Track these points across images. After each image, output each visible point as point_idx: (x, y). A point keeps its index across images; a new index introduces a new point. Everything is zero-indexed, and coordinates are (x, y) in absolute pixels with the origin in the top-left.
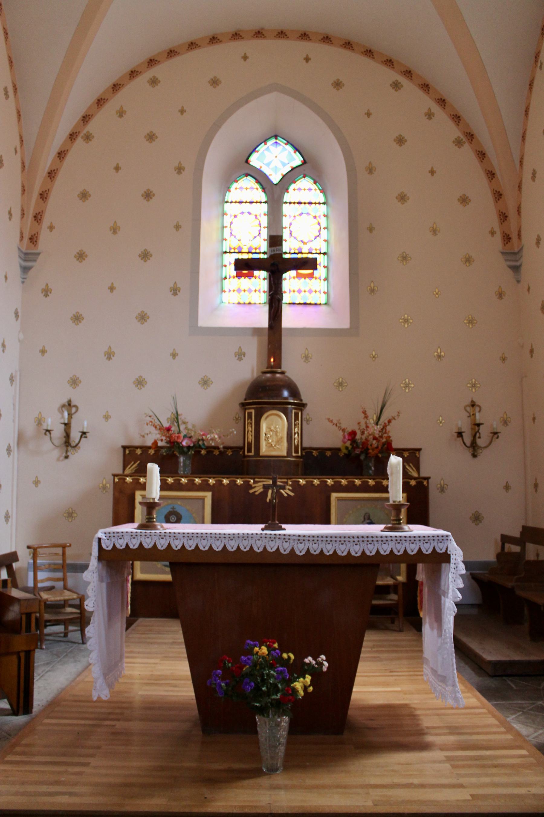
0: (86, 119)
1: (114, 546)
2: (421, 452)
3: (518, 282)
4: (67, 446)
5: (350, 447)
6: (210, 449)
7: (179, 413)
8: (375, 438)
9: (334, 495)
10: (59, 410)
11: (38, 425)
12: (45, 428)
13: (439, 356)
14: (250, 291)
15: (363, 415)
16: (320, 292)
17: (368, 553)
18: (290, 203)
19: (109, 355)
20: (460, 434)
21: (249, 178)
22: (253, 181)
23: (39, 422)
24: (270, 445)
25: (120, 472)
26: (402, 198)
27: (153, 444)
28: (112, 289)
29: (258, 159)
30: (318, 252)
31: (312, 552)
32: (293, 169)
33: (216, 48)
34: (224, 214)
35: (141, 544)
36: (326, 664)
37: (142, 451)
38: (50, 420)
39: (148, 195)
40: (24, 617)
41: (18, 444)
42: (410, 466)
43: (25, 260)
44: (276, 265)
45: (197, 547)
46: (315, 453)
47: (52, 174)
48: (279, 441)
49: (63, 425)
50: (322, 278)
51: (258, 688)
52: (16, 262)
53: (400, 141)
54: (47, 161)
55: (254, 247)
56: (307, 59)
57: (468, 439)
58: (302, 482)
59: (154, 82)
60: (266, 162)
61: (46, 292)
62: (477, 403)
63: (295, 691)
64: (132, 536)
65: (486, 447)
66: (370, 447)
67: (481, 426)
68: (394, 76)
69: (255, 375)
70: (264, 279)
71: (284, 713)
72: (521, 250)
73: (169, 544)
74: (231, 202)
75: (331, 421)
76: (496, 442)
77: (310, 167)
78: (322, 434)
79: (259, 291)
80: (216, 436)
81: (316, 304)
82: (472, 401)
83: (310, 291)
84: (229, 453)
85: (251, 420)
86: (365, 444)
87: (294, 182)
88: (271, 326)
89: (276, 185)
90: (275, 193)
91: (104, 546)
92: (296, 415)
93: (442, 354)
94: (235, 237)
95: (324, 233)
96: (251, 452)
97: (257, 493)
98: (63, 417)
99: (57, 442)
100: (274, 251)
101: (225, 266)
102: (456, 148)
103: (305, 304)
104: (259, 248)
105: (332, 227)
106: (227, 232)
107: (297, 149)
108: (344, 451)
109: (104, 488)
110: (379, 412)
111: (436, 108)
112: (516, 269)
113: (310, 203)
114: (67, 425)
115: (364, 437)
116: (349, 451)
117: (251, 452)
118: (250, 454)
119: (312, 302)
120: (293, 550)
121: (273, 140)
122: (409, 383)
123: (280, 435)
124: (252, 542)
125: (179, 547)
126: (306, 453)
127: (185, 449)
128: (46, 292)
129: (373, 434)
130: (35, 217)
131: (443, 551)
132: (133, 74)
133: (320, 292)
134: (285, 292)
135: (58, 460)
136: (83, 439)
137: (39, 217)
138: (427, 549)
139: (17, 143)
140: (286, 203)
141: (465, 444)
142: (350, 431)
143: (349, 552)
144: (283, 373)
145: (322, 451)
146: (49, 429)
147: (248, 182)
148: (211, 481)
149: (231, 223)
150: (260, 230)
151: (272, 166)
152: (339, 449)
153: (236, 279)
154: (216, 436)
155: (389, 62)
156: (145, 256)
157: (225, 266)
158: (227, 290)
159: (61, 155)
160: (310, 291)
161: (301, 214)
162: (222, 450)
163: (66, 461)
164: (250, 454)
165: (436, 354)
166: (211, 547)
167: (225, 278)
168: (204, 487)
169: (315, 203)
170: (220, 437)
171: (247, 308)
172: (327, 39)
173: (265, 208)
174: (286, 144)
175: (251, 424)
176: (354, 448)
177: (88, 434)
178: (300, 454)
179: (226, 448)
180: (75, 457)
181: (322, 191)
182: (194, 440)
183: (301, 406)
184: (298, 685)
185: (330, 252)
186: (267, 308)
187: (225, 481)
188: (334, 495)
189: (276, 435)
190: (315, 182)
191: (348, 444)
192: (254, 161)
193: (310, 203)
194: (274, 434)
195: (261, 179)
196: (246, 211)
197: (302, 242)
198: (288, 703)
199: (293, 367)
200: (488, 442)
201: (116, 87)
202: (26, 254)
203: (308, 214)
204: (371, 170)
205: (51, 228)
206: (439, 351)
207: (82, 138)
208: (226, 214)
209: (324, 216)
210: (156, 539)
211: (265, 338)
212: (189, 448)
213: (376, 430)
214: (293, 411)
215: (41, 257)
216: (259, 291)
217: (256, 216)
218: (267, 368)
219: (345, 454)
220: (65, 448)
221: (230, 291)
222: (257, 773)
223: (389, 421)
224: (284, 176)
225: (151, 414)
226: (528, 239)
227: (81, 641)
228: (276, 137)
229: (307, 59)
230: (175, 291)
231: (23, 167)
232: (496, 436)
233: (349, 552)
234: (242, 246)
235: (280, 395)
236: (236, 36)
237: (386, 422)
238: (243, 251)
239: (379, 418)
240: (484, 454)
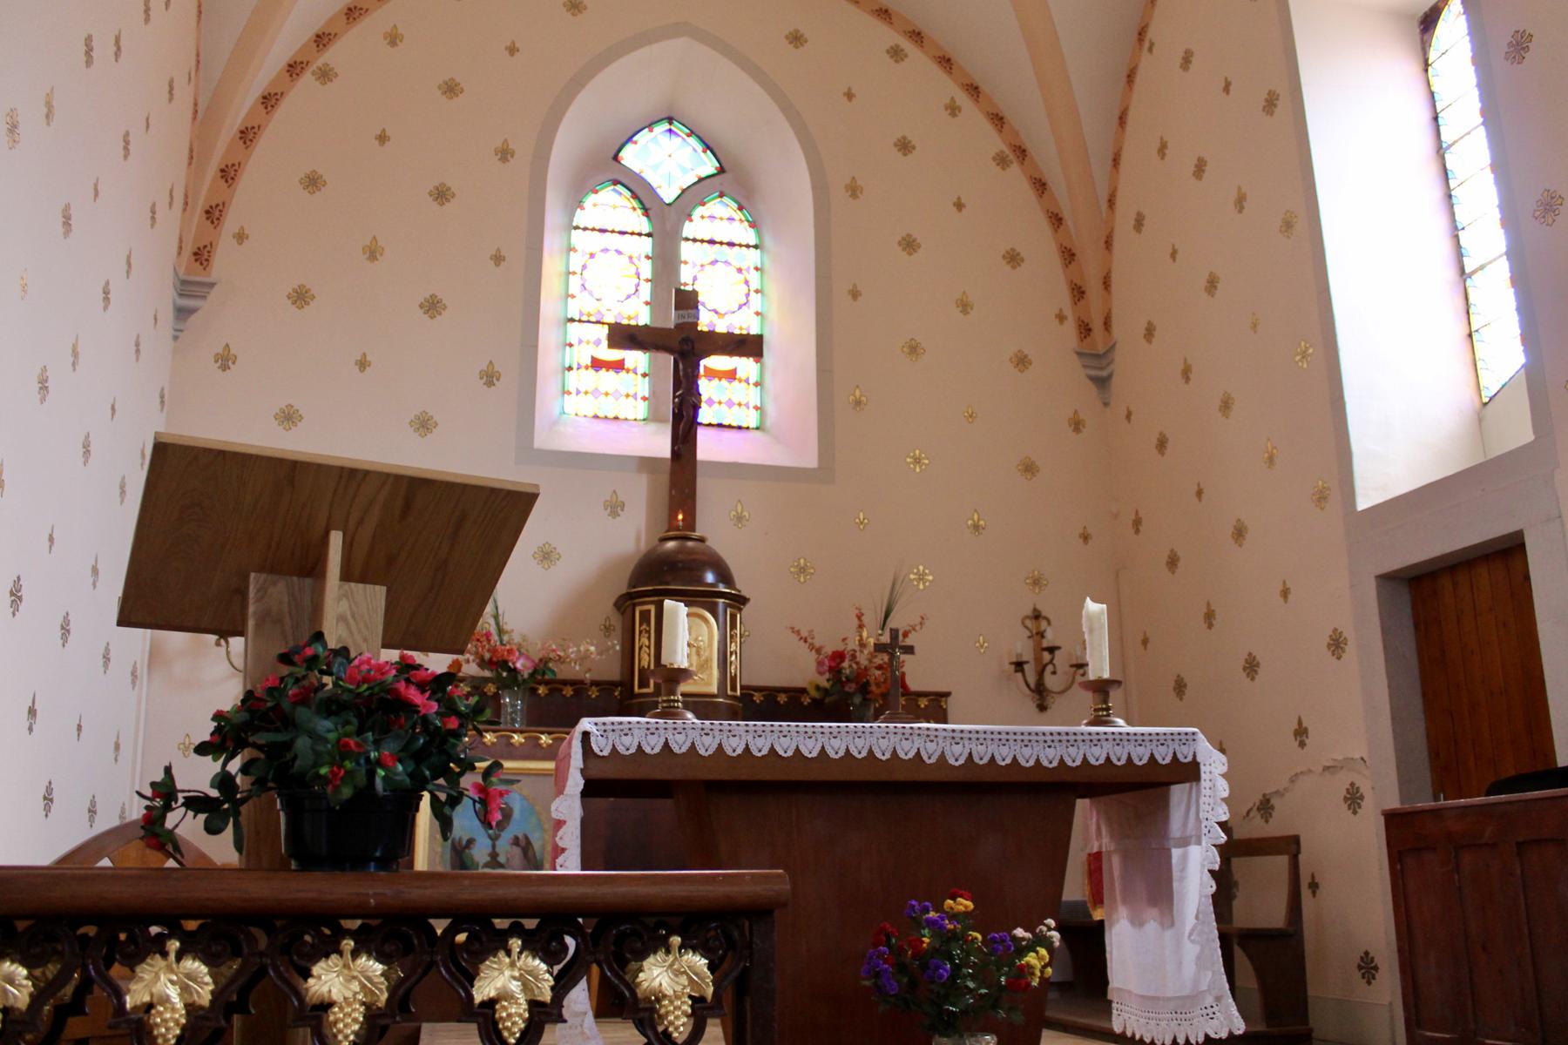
0: (322, 40)
2: (950, 699)
3: (1106, 404)
13: (976, 527)
20: (1019, 666)
28: (363, 364)
32: (701, 180)
34: (571, 249)
35: (666, 744)
43: (181, 295)
44: (680, 344)
45: (772, 750)
47: (247, 135)
50: (752, 381)
52: (167, 299)
61: (225, 360)
65: (1063, 692)
67: (1057, 653)
68: (892, 37)
69: (643, 547)
70: (644, 375)
73: (720, 745)
77: (730, 178)
81: (740, 428)
82: (1035, 610)
83: (730, 404)
85: (649, 625)
92: (733, 617)
94: (591, 293)
95: (754, 298)
96: (647, 686)
101: (571, 345)
102: (998, 169)
103: (720, 425)
105: (772, 289)
106: (575, 282)
107: (708, 147)
111: (963, 99)
112: (1102, 383)
113: (731, 244)
117: (647, 686)
118: (645, 690)
119: (734, 424)
120: (943, 756)
121: (666, 126)
123: (705, 655)
125: (739, 751)
128: (225, 360)
130: (207, 212)
131: (1190, 759)
139: (193, 63)
140: (687, 239)
144: (702, 540)
149: (584, 267)
152: (803, 691)
153: (591, 371)
156: (432, 306)
157: (571, 345)
158: (574, 392)
159: (269, 101)
160: (730, 404)
161: (714, 263)
164: (645, 690)
166: (797, 750)
167: (570, 369)
171: (613, 426)
173: (646, 245)
175: (648, 632)
181: (752, 225)
189: (698, 654)
190: (741, 208)
192: (629, 157)
193: (731, 244)
195: (642, 194)
196: (612, 247)
199: (717, 525)
200: (1062, 688)
202: (184, 282)
204: (854, 190)
205: (241, 237)
207: (313, 73)
208: (575, 250)
209: (757, 269)
211: (665, 479)
215: (214, 294)
219: (814, 700)
221: (578, 392)
224: (684, 191)
226: (1126, 329)
228: (670, 120)
230: (490, 378)
233: (1038, 760)
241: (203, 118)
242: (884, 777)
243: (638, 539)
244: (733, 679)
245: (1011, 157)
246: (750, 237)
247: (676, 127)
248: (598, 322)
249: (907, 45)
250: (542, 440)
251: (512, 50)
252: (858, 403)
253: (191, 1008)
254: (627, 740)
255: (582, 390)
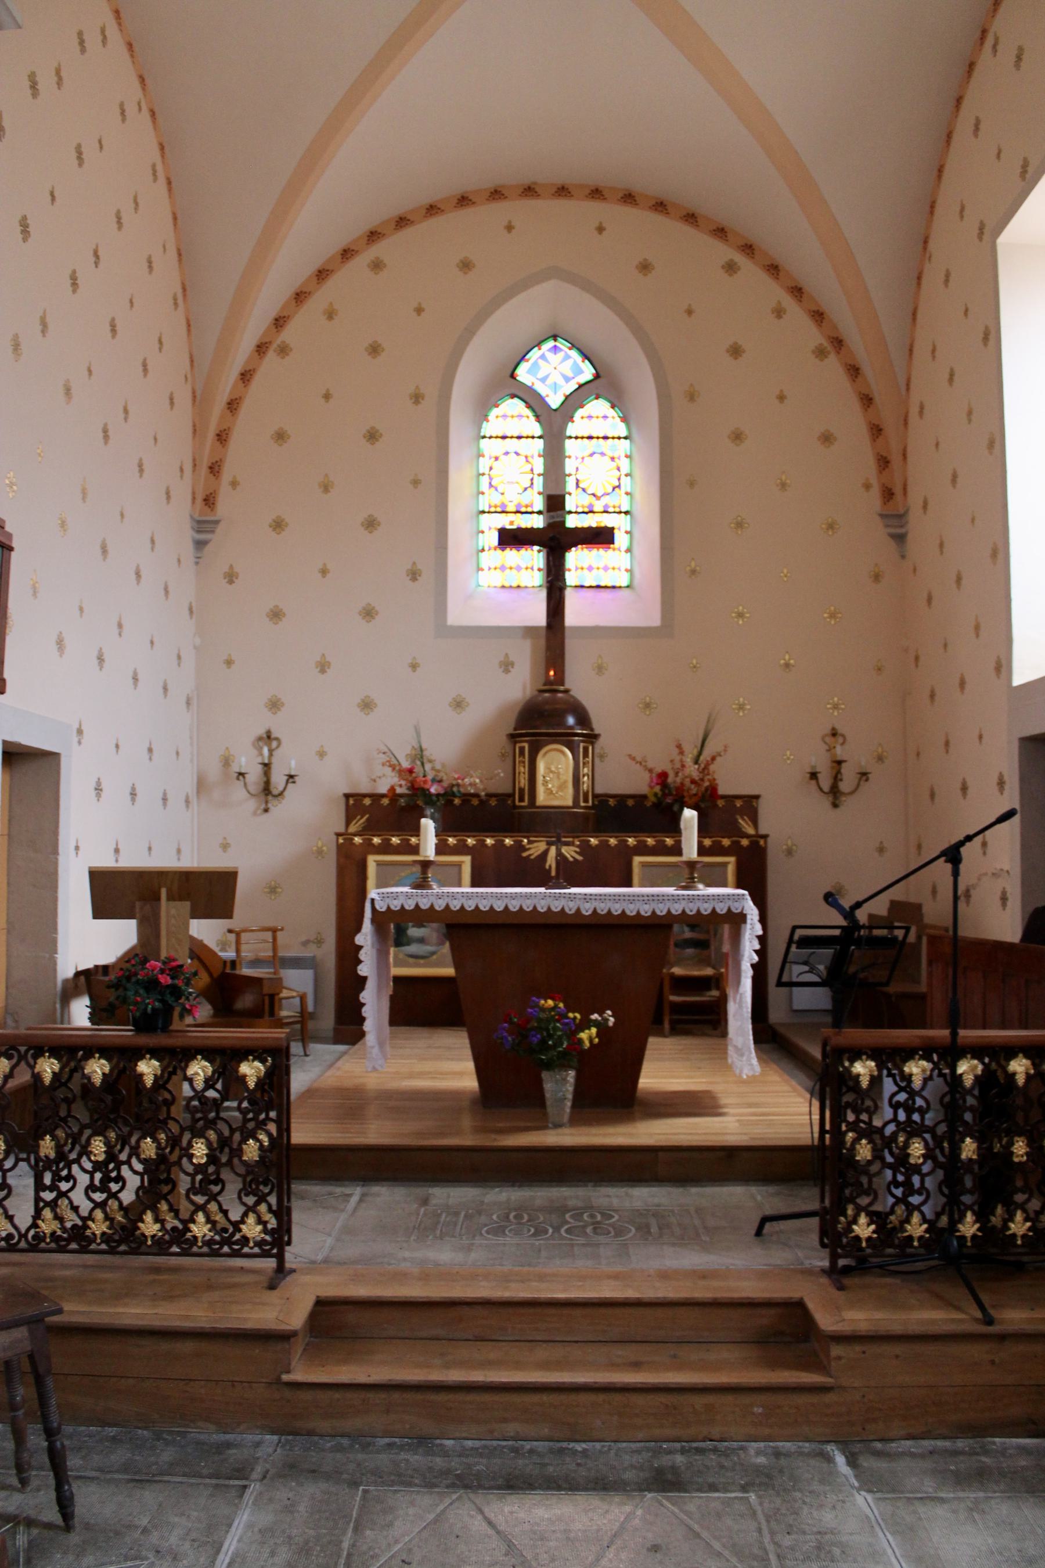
0: (279, 322)
1: (389, 907)
2: (760, 800)
3: (903, 557)
4: (267, 795)
5: (660, 794)
6: (467, 797)
7: (424, 747)
8: (693, 782)
9: (637, 860)
10: (253, 745)
11: (224, 766)
12: (238, 770)
13: (787, 665)
14: (519, 568)
15: (677, 751)
16: (619, 569)
17: (659, 913)
18: (576, 438)
19: (323, 667)
21: (516, 400)
22: (522, 404)
23: (227, 762)
24: (549, 792)
25: (342, 830)
26: (737, 437)
27: (389, 791)
28: (324, 572)
29: (529, 372)
30: (617, 510)
31: (599, 911)
33: (467, 214)
36: (612, 1019)
37: (373, 800)
38: (243, 760)
39: (372, 436)
40: (267, 999)
41: (198, 792)
42: (743, 820)
43: (199, 532)
46: (612, 802)
47: (233, 405)
48: (562, 787)
49: (260, 766)
51: (544, 1042)
52: (188, 535)
53: (736, 351)
54: (227, 384)
55: (523, 504)
56: (600, 229)
57: (826, 783)
58: (593, 841)
59: (377, 266)
60: (540, 375)
61: (231, 577)
62: (840, 731)
63: (581, 1041)
64: (408, 896)
66: (685, 794)
67: (843, 765)
68: (725, 252)
69: (529, 693)
71: (571, 1067)
72: (907, 512)
74: (490, 437)
75: (634, 759)
76: (865, 787)
77: (604, 384)
78: (621, 775)
79: (532, 569)
80: (477, 781)
81: (614, 587)
82: (833, 729)
84: (493, 802)
86: (681, 788)
87: (582, 407)
88: (550, 626)
89: (555, 410)
90: (554, 423)
91: (378, 907)
92: (586, 750)
93: (792, 662)
97: (532, 857)
98: (261, 754)
99: (252, 789)
100: (553, 517)
101: (483, 532)
103: (598, 587)
104: (532, 506)
105: (637, 473)
106: (484, 481)
107: (586, 357)
108: (653, 799)
109: (320, 852)
110: (699, 746)
111: (788, 302)
113: (605, 438)
114: (267, 766)
115: (678, 780)
116: (658, 799)
118: (522, 804)
119: (609, 585)
120: (578, 910)
121: (551, 343)
122: (744, 704)
123: (563, 778)
124: (535, 901)
126: (599, 801)
127: (434, 798)
128: (231, 577)
129: (690, 776)
130: (211, 468)
132: (347, 254)
133: (619, 569)
134: (569, 570)
135: (255, 814)
136: (290, 785)
137: (217, 468)
138: (721, 909)
140: (570, 437)
141: (821, 789)
142: (660, 771)
143: (638, 912)
144: (566, 691)
145: (622, 798)
146: (243, 771)
147: (514, 406)
148: (470, 841)
149: (491, 468)
150: (532, 479)
151: (549, 381)
152: (644, 797)
153: (499, 551)
154: (477, 781)
155: (721, 232)
157: (483, 532)
158: (486, 569)
159: (246, 376)
161: (591, 455)
162: (484, 798)
163: (266, 815)
164: (522, 804)
165: (782, 662)
167: (483, 550)
168: (461, 849)
169: (613, 438)
170: (481, 781)
171: (516, 591)
172: (629, 198)
173: (540, 444)
174: (570, 349)
176: (665, 795)
177: (296, 778)
178: (590, 804)
179: (490, 795)
180: (278, 809)
181: (624, 419)
182: (445, 784)
183: (592, 738)
184: (584, 1035)
185: (634, 511)
186: (543, 594)
187: (489, 841)
188: (637, 860)
189: (558, 778)
190: (613, 407)
191: (657, 789)
192: (523, 374)
193: (605, 438)
194: (555, 777)
196: (512, 450)
197: (594, 495)
198: (575, 1056)
199: (581, 682)
201: (322, 274)
202: (199, 522)
203: (603, 454)
204: (692, 397)
205: (234, 484)
206: (787, 657)
209: (627, 456)
210: (433, 899)
211: (542, 642)
212: (438, 795)
213: (692, 770)
214: (582, 745)
215: (220, 529)
216: (532, 569)
217: (526, 457)
218: (545, 685)
220: (263, 797)
222: (546, 1128)
223: (713, 759)
224: (567, 397)
225: (386, 750)
226: (915, 499)
227: (302, 1053)
228: (555, 338)
229: (600, 229)
231: (194, 397)
232: (864, 778)
234: (506, 503)
235: (562, 723)
236: (496, 194)
237: (709, 759)
238: (508, 509)
239: (700, 754)
240: (849, 804)
241: (199, 400)
242: (542, 921)
243: (524, 688)
244: (586, 795)
245: (829, 348)
246: (622, 430)
247: (561, 344)
248: (503, 512)
249: (739, 258)
250: (457, 615)
251: (419, 310)
252: (693, 572)
253: (104, 1074)
254: (395, 902)
255: (492, 567)
